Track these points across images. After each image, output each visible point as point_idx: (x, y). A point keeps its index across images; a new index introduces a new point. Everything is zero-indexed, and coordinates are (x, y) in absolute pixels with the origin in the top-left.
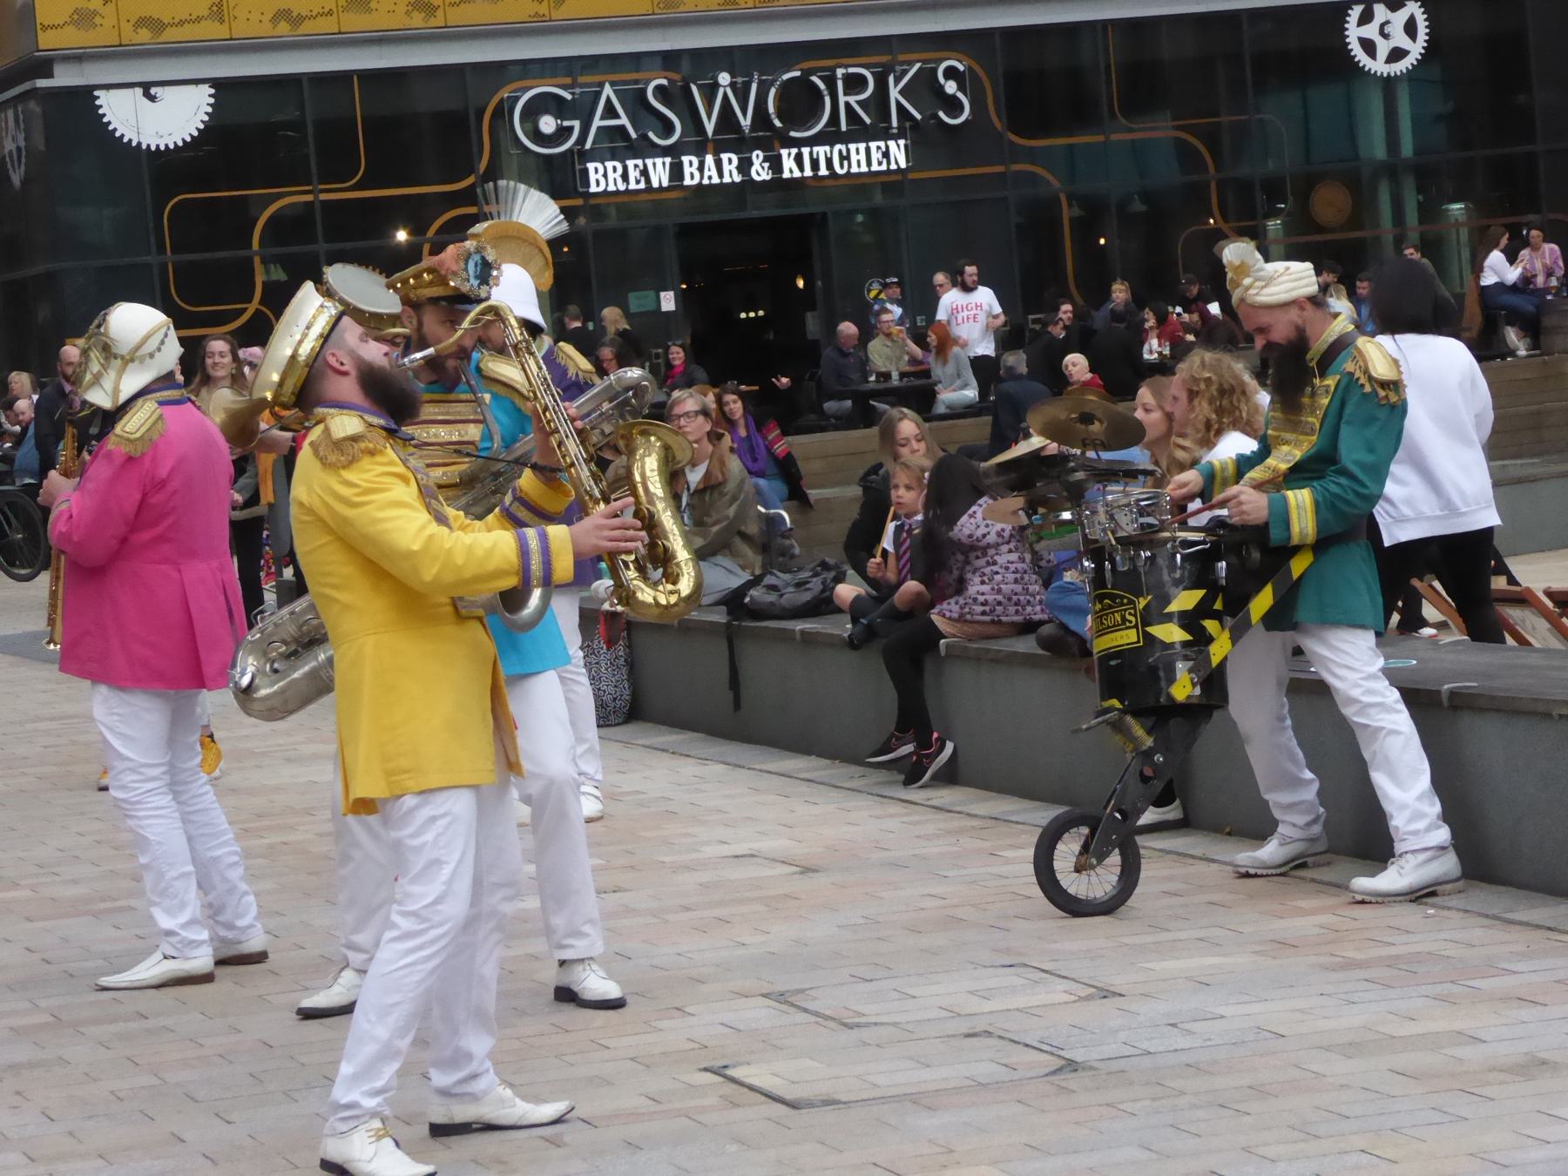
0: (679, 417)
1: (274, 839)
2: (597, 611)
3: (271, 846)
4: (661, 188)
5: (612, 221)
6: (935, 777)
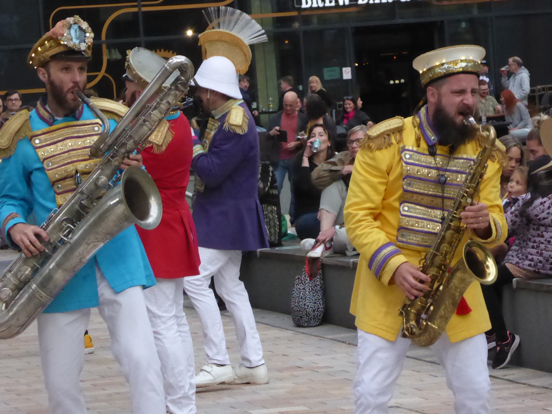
0: (353, 141)
1: (111, 391)
2: (305, 258)
3: (110, 395)
4: (344, 6)
5: (315, 25)
6: (509, 363)
